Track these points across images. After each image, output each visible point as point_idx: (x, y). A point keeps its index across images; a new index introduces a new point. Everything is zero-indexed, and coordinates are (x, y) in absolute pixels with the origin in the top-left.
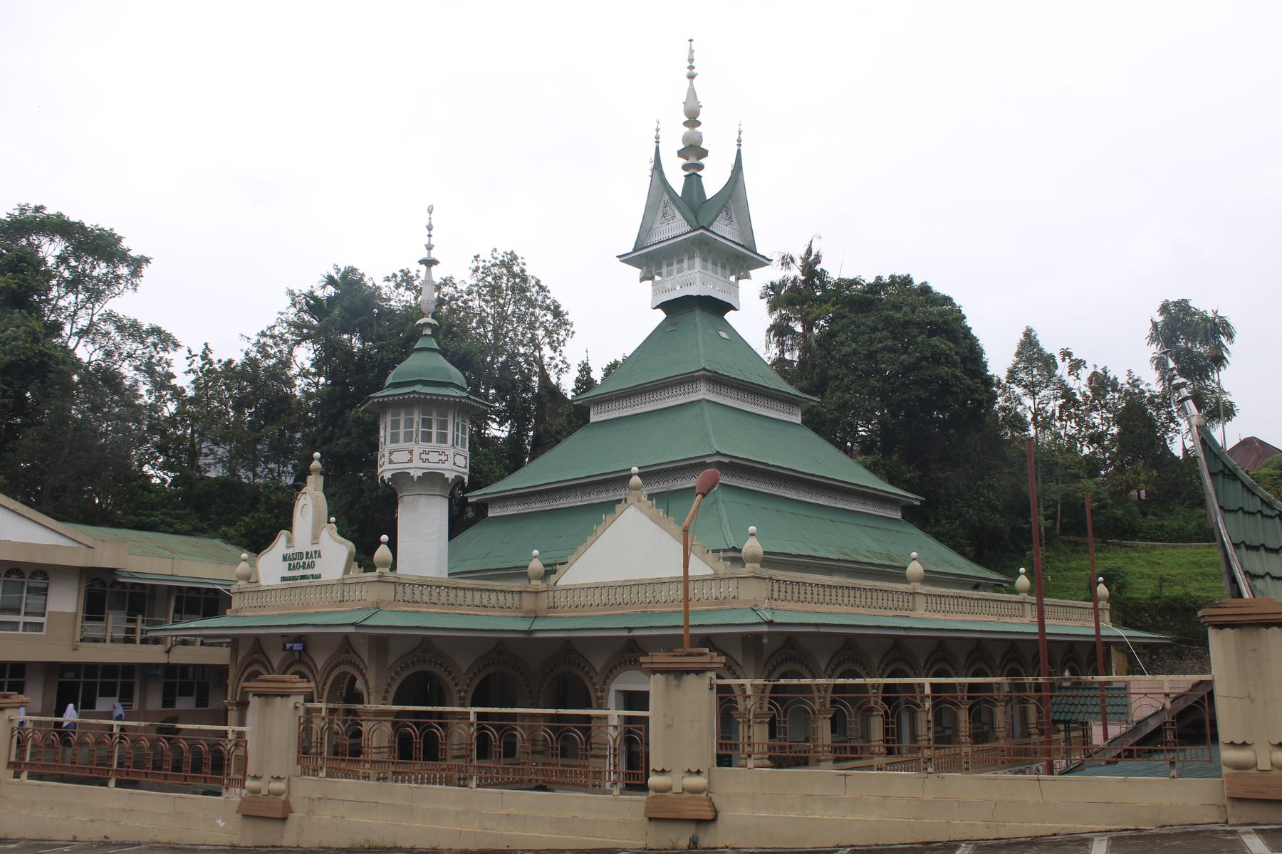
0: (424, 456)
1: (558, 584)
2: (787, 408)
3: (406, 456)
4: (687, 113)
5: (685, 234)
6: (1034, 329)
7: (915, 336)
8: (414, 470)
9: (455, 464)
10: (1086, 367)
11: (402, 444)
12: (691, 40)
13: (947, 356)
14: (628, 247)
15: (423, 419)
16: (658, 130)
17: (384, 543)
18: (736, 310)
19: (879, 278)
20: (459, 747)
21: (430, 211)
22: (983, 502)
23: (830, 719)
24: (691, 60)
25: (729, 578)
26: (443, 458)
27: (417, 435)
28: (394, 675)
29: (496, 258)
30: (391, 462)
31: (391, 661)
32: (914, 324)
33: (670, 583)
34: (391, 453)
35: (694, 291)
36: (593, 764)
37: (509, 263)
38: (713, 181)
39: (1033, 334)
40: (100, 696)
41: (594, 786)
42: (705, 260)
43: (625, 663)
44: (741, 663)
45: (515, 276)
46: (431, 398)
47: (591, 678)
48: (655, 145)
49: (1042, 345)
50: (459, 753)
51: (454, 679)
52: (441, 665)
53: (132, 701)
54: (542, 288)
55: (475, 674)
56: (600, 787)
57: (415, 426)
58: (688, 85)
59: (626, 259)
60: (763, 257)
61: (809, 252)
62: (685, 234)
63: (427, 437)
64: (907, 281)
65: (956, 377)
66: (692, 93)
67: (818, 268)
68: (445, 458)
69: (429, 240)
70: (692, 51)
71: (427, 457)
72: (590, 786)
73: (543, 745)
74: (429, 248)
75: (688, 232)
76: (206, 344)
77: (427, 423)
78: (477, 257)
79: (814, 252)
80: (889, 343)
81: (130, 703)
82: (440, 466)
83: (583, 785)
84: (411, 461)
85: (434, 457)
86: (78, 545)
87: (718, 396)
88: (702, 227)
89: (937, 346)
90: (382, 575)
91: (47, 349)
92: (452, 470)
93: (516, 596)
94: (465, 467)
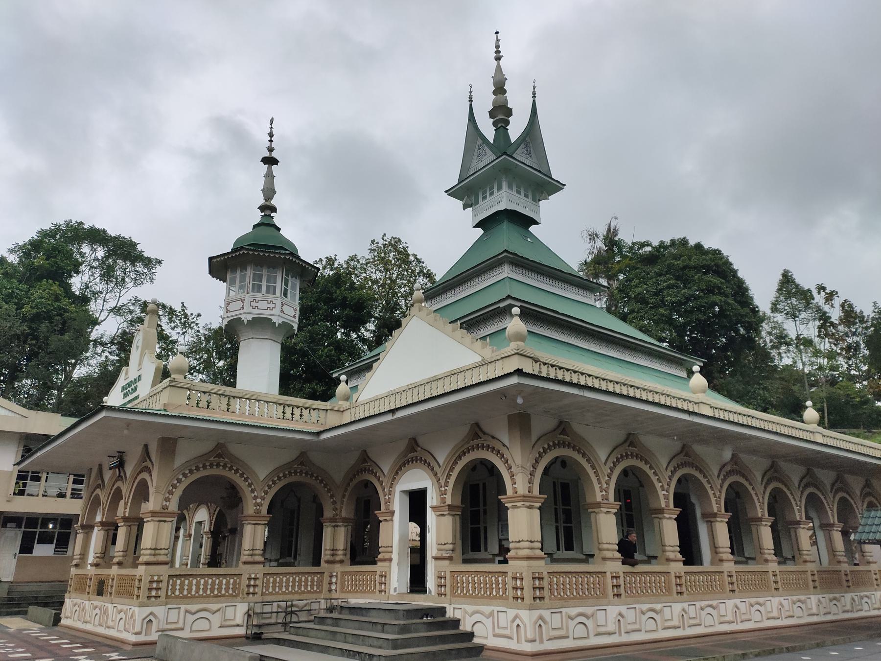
0: (254, 304)
2: (581, 292)
3: (240, 304)
4: (469, 98)
5: (492, 162)
6: (791, 270)
7: (693, 276)
8: (244, 315)
9: (282, 311)
10: (838, 296)
12: (497, 33)
13: (719, 288)
14: (453, 180)
15: (254, 274)
16: (471, 92)
18: (537, 223)
19: (662, 242)
22: (760, 400)
24: (497, 47)
26: (272, 306)
27: (248, 287)
29: (386, 241)
32: (691, 268)
33: (444, 378)
35: (501, 207)
36: (380, 567)
37: (395, 244)
38: (516, 129)
39: (790, 274)
40: (38, 543)
41: (380, 591)
42: (510, 187)
43: (408, 462)
44: (507, 444)
45: (399, 252)
46: (264, 255)
48: (469, 103)
49: (798, 281)
50: (250, 559)
51: (250, 485)
53: (67, 548)
54: (419, 261)
57: (247, 280)
59: (452, 192)
60: (558, 182)
61: (609, 229)
62: (492, 162)
63: (257, 288)
64: (684, 242)
65: (729, 304)
66: (499, 69)
67: (616, 238)
69: (271, 144)
70: (498, 40)
71: (256, 304)
72: (511, 599)
73: (343, 555)
74: (271, 150)
75: (494, 160)
76: (182, 303)
78: (373, 241)
79: (612, 227)
80: (672, 282)
81: (66, 550)
82: (268, 312)
84: (242, 308)
85: (263, 305)
86: (13, 415)
87: (521, 276)
88: (505, 153)
89: (711, 281)
90: (174, 380)
91: (64, 305)
92: (279, 316)
94: (294, 317)
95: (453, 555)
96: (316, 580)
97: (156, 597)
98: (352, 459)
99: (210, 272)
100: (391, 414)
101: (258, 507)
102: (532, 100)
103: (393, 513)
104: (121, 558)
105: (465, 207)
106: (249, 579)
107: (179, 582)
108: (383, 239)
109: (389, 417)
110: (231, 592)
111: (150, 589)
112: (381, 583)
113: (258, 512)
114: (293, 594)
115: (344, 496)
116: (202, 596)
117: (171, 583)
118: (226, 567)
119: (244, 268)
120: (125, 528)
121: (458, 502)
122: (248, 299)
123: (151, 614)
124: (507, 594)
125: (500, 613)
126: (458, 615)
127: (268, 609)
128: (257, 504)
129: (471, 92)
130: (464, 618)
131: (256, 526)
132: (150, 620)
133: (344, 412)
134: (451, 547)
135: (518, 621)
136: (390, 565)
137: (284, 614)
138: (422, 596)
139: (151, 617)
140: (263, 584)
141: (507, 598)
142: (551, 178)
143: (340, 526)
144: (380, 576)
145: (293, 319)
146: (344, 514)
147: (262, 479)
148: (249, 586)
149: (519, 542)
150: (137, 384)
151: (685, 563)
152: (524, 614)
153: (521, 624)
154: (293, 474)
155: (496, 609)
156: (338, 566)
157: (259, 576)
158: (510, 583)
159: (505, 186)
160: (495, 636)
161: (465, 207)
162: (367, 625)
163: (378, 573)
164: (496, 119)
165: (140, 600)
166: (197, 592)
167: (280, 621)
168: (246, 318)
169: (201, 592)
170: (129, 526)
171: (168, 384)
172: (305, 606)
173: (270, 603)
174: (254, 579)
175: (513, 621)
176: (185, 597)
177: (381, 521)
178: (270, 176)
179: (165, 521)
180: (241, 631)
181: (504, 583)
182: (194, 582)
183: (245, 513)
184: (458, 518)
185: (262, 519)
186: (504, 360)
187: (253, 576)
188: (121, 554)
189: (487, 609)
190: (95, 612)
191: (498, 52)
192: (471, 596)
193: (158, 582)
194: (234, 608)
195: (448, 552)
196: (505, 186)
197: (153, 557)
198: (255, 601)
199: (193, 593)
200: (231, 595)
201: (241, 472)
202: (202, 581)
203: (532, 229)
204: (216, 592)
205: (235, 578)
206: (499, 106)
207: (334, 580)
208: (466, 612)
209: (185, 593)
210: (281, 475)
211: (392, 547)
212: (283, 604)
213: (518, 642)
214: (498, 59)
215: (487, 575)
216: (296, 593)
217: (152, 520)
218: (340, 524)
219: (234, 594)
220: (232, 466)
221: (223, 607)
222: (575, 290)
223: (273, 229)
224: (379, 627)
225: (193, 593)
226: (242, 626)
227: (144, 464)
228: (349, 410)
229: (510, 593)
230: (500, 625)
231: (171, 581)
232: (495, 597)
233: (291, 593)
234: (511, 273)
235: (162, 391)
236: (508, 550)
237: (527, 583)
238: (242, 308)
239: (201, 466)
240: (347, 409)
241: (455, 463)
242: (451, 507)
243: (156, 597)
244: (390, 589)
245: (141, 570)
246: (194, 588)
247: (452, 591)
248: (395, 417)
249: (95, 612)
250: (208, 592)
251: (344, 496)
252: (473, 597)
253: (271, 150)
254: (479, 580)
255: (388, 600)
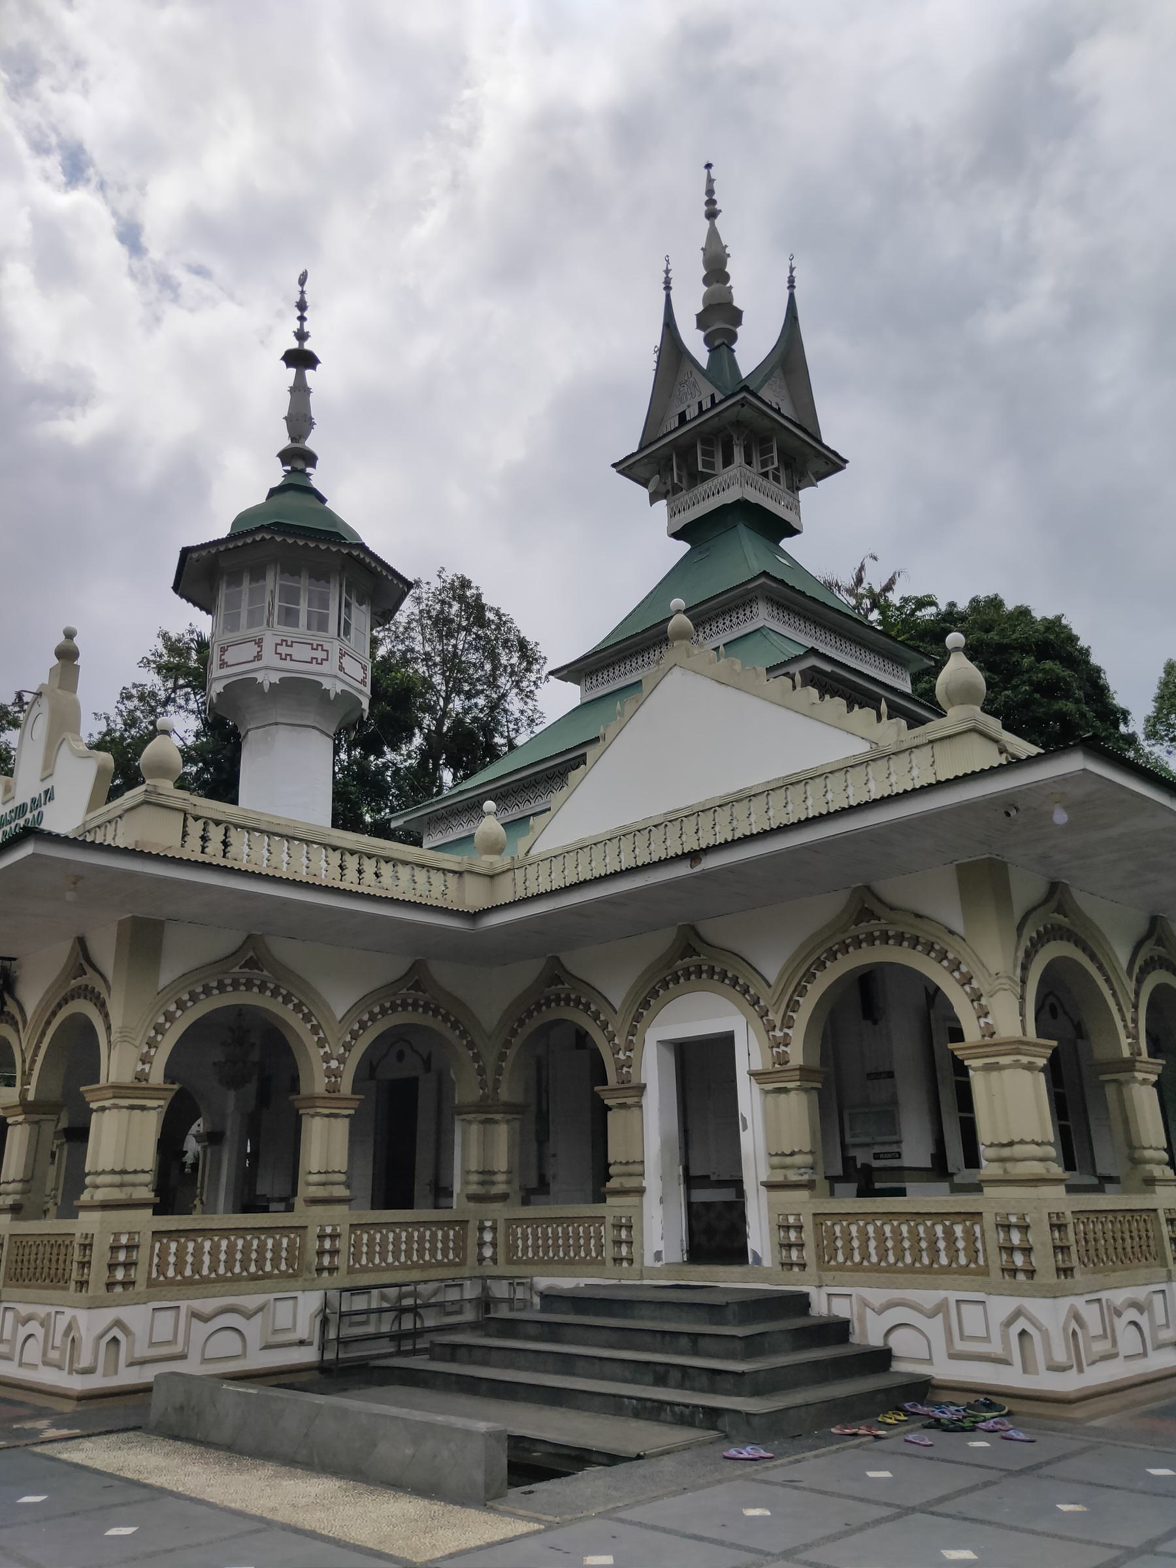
0: (283, 650)
1: (532, 853)
2: (889, 666)
3: (252, 649)
4: (708, 263)
8: (264, 672)
9: (341, 668)
11: (244, 632)
12: (708, 166)
14: (630, 444)
17: (956, 649)
20: (322, 1178)
21: (302, 281)
23: (1156, 1085)
24: (710, 192)
25: (910, 749)
26: (320, 655)
27: (270, 614)
28: (173, 1008)
30: (223, 664)
31: (166, 978)
33: (768, 792)
34: (223, 650)
35: (729, 497)
41: (618, 1260)
47: (604, 1026)
50: (320, 1192)
52: (287, 1000)
55: (363, 1026)
56: (631, 1261)
57: (268, 598)
58: (708, 226)
63: (289, 617)
66: (713, 235)
68: (323, 655)
69: (302, 325)
70: (710, 181)
71: (288, 650)
72: (610, 1263)
74: (301, 336)
77: (291, 596)
82: (314, 667)
83: (593, 1262)
84: (258, 657)
90: (154, 791)
93: (452, 880)
94: (363, 682)
95: (814, 1177)
96: (451, 1237)
97: (127, 1284)
98: (528, 973)
99: (176, 588)
100: (688, 863)
101: (333, 1079)
102: (787, 292)
103: (641, 1089)
104: (18, 1197)
105: (654, 498)
106: (321, 1237)
107: (173, 1246)
108: (440, 576)
109: (683, 870)
110: (283, 1267)
111: (112, 1267)
112: (618, 1243)
113: (333, 1089)
114: (396, 1269)
115: (502, 1057)
116: (221, 1279)
117: (157, 1251)
118: (204, 1212)
119: (258, 574)
120: (27, 1127)
121: (815, 1062)
122: (269, 641)
123: (118, 1323)
124: (981, 1261)
125: (963, 1307)
126: (841, 1309)
127: (360, 1303)
128: (330, 1073)
129: (667, 271)
130: (862, 1319)
131: (332, 1120)
132: (115, 1340)
133: (496, 878)
134: (809, 1159)
135: (1021, 1324)
136: (641, 1203)
137: (393, 1314)
138: (736, 1270)
139: (116, 1332)
140: (349, 1248)
141: (985, 1271)
142: (820, 442)
143: (496, 1122)
144: (614, 1226)
145: (361, 687)
146: (504, 1094)
147: (339, 1017)
148: (321, 1253)
149: (1011, 1144)
150: (43, 808)
151: (159, 1210)
152: (1037, 1307)
153: (1030, 1329)
154: (421, 1010)
155: (953, 1296)
156: (497, 1206)
157: (343, 1229)
158: (607, 1233)
159: (738, 456)
160: (954, 1356)
161: (654, 498)
162: (648, 1339)
163: (610, 1220)
164: (709, 330)
165: (90, 1293)
166: (213, 1268)
167: (385, 1328)
168: (268, 678)
169: (221, 1270)
170: (37, 1123)
171: (141, 798)
172: (435, 1293)
173: (365, 1290)
174: (330, 1236)
175: (1009, 1323)
176: (187, 1282)
177: (610, 1109)
178: (300, 391)
179: (143, 1108)
180: (308, 1355)
181: (599, 1237)
182: (207, 1245)
183: (304, 1090)
184: (815, 1095)
185: (344, 1104)
186: (937, 746)
187: (329, 1230)
188: (18, 1186)
189: (929, 1297)
190: (23, 1332)
191: (711, 202)
192: (876, 1268)
193: (129, 1248)
194: (291, 1302)
195: (803, 1170)
196: (738, 456)
197: (117, 1189)
198: (341, 1286)
199: (205, 1272)
200: (284, 1275)
201: (296, 1001)
202: (224, 1244)
203: (786, 544)
204: (253, 1269)
205: (292, 1236)
206: (719, 304)
207: (488, 1237)
208: (865, 1304)
209: (188, 1272)
210: (377, 1010)
211: (642, 1162)
212: (392, 1292)
213: (1025, 1371)
214: (712, 215)
215: (920, 1220)
216: (415, 1266)
217: (116, 1106)
218: (497, 1117)
219: (291, 1271)
220: (277, 987)
221: (269, 1300)
222: (879, 661)
223: (312, 498)
224: (684, 1342)
225: (205, 1272)
226: (311, 1344)
227: (80, 981)
228: (511, 874)
229: (997, 1261)
230: (966, 1334)
231: (157, 1245)
232: (946, 1270)
233: (404, 1267)
234: (770, 619)
235: (120, 817)
236: (609, 1177)
237: (1041, 1238)
238: (258, 657)
239: (215, 984)
240: (504, 872)
241: (810, 976)
242: (805, 1072)
243: (127, 1284)
244: (642, 1255)
245: (88, 1222)
246: (206, 1259)
247: (820, 1258)
248: (698, 868)
249: (23, 1332)
250: (237, 1270)
251: (502, 1057)
252: (864, 1270)
253: (301, 336)
254: (555, 1232)
255: (641, 1278)
